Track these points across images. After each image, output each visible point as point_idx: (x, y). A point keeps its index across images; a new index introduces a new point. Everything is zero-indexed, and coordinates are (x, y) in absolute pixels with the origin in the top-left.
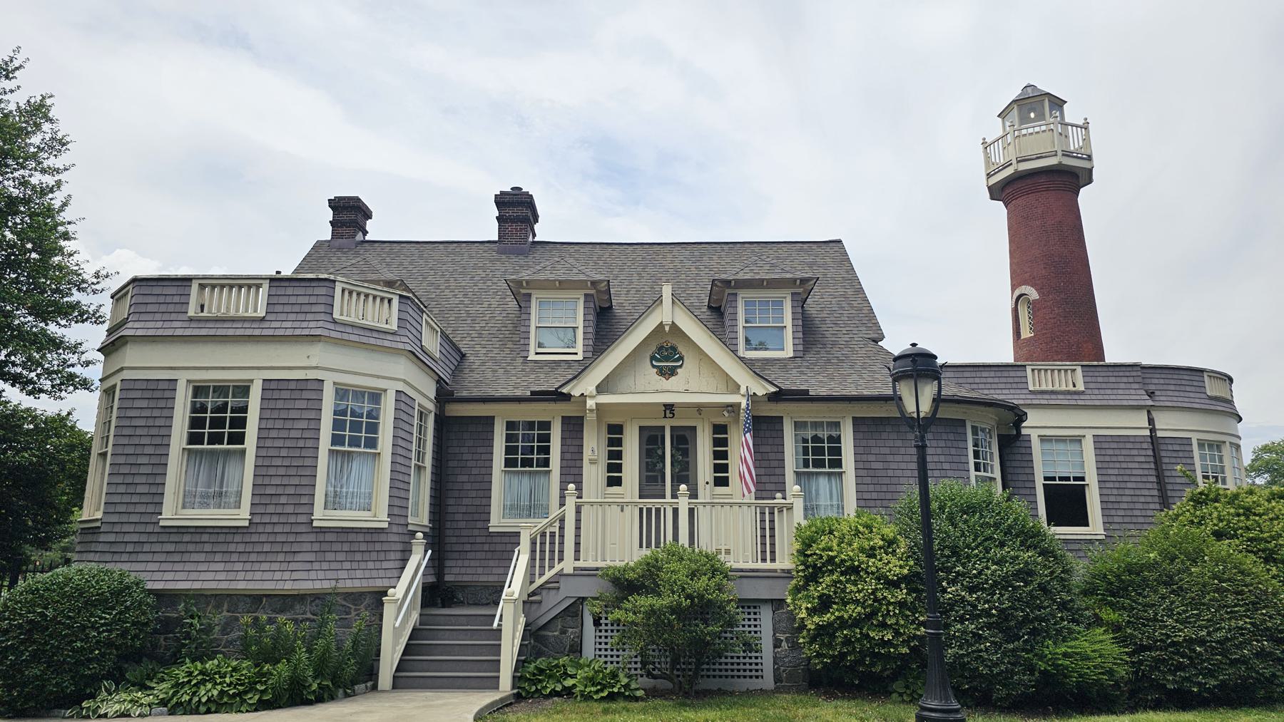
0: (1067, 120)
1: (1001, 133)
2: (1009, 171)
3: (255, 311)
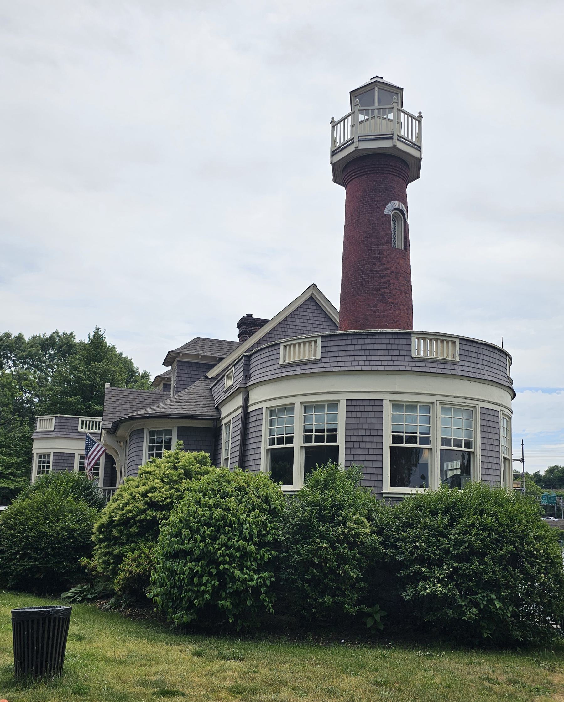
2: (352, 149)
3: (315, 355)
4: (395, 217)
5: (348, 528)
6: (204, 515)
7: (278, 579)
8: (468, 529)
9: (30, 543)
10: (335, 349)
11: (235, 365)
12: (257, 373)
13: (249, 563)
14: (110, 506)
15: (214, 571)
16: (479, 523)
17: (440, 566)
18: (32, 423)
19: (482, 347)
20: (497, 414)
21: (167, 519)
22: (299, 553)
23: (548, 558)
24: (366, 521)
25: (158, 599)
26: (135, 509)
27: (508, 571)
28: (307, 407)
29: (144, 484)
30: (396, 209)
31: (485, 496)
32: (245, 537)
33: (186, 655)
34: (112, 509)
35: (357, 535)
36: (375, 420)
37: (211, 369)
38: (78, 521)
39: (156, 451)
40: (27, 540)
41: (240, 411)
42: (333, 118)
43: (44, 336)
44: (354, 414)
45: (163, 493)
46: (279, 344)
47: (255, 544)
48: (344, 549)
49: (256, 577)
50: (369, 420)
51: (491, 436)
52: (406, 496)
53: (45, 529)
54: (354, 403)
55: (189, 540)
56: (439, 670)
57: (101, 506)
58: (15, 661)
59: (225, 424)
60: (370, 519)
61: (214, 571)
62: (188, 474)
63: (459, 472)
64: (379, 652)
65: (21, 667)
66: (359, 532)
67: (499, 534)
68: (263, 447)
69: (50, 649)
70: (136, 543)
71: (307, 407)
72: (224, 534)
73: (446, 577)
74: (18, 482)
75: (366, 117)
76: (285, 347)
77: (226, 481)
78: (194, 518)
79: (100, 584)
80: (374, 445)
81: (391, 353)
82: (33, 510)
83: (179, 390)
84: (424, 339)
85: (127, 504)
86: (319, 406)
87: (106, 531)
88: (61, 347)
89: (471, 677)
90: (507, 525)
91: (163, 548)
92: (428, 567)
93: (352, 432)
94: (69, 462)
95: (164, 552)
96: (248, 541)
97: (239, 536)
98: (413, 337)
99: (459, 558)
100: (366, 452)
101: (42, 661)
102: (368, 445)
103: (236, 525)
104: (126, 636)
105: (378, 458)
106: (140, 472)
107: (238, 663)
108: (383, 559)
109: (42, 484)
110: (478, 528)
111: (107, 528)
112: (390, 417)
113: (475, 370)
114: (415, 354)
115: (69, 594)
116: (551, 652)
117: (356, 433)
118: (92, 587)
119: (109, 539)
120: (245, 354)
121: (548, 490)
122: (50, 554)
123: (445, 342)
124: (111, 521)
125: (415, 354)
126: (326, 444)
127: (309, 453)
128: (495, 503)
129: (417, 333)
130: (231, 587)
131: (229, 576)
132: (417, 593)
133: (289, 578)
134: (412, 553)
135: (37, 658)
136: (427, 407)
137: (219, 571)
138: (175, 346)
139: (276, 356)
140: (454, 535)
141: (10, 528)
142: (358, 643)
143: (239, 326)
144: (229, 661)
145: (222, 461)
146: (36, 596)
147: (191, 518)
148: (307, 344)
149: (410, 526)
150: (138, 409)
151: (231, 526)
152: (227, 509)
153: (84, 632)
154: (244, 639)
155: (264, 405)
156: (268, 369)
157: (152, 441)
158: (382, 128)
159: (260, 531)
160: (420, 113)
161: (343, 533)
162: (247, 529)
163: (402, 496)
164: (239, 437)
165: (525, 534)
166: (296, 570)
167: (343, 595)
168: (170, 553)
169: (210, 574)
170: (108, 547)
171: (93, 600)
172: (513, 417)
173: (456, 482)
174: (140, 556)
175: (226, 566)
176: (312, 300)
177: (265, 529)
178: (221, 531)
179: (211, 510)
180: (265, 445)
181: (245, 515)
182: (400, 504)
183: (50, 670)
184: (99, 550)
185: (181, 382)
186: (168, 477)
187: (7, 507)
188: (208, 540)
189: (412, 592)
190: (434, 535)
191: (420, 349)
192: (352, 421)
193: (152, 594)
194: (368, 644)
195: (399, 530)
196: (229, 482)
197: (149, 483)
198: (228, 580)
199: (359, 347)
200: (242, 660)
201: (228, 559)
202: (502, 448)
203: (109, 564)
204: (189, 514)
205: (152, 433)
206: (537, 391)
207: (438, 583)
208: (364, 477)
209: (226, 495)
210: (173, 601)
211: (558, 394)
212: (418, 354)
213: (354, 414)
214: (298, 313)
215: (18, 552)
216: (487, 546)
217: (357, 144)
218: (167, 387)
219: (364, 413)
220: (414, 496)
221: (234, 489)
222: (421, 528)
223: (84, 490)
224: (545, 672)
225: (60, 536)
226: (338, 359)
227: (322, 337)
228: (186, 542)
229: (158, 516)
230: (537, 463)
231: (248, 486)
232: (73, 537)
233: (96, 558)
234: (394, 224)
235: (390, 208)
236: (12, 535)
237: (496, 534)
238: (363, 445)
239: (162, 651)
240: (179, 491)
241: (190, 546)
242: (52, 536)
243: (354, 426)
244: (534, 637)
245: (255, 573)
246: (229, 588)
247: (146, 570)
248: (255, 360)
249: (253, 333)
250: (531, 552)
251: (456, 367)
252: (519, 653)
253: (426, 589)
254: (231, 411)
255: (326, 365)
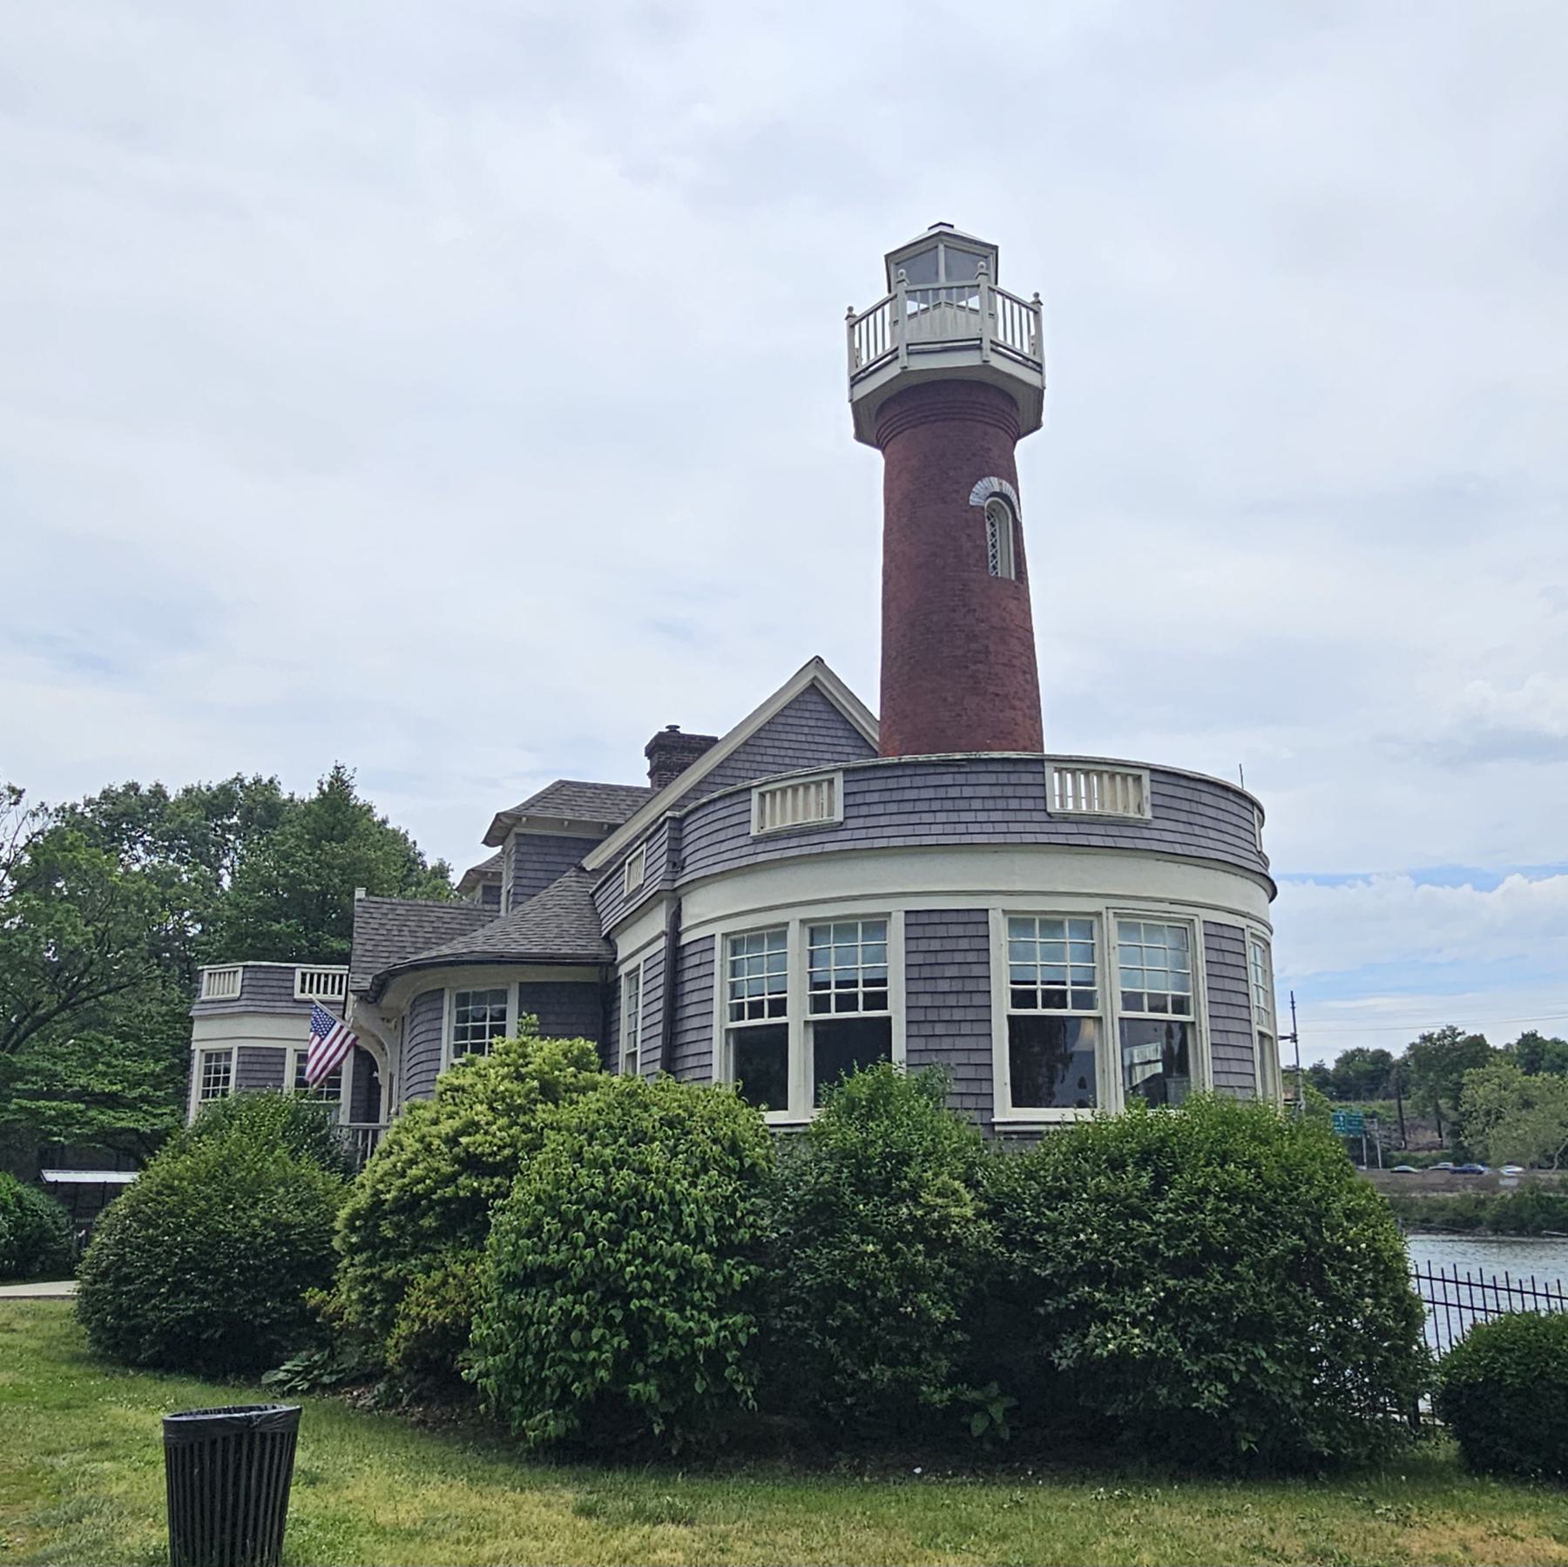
0: (1001, 285)
1: (885, 294)
2: (894, 370)
3: (831, 814)
4: (993, 512)
5: (924, 1206)
6: (592, 1186)
7: (766, 1330)
8: (1195, 1198)
9: (191, 1257)
10: (875, 797)
11: (647, 840)
12: (699, 855)
13: (697, 1296)
14: (374, 1169)
15: (618, 1315)
16: (1218, 1185)
17: (1136, 1287)
18: (191, 981)
19: (1200, 786)
20: (1239, 935)
21: (506, 1196)
22: (811, 1269)
23: (1377, 1260)
24: (962, 1190)
25: (489, 1383)
26: (432, 1175)
27: (1289, 1293)
28: (816, 930)
29: (450, 1117)
30: (994, 494)
31: (1230, 1121)
32: (687, 1235)
33: (560, 1513)
34: (378, 1175)
35: (945, 1221)
36: (971, 957)
37: (590, 851)
38: (299, 1204)
39: (473, 1039)
40: (183, 1249)
41: (662, 943)
42: (850, 309)
43: (209, 789)
44: (923, 945)
45: (494, 1135)
46: (749, 789)
47: (710, 1249)
48: (917, 1255)
49: (714, 1325)
50: (959, 957)
51: (1229, 985)
52: (1051, 1128)
53: (225, 1224)
54: (924, 919)
55: (559, 1243)
56: (1150, 1532)
57: (349, 1171)
58: (172, 1540)
59: (627, 975)
60: (971, 1183)
61: (618, 1315)
62: (549, 1091)
63: (1159, 1068)
64: (1002, 1495)
65: (186, 1554)
66: (949, 1215)
67: (1268, 1211)
68: (717, 1026)
69: (252, 1506)
70: (434, 1251)
71: (816, 930)
72: (638, 1227)
73: (1151, 1313)
74: (155, 1116)
75: (923, 306)
76: (762, 795)
77: (638, 1106)
78: (569, 1191)
79: (348, 1349)
80: (971, 1014)
81: (1001, 804)
82: (199, 1181)
83: (520, 899)
84: (1073, 772)
85: (412, 1162)
86: (845, 927)
87: (364, 1226)
88: (250, 811)
89: (1222, 1547)
90: (1282, 1187)
91: (499, 1263)
92: (1107, 1291)
93: (919, 986)
94: (273, 1068)
95: (501, 1273)
96: (694, 1243)
97: (675, 1232)
98: (1049, 768)
99: (1179, 1268)
100: (953, 1030)
101: (234, 1538)
102: (958, 1015)
103: (666, 1207)
104: (418, 1473)
105: (983, 1044)
106: (439, 1088)
107: (683, 1531)
108: (1004, 1274)
109: (216, 1119)
110: (1217, 1197)
111: (366, 1219)
112: (1006, 949)
113: (1188, 839)
114: (1054, 806)
115: (281, 1376)
116: (1399, 1478)
117: (930, 986)
118: (332, 1357)
119: (372, 1245)
120: (669, 814)
121: (1344, 1103)
122: (238, 1283)
123: (1118, 778)
124: (377, 1204)
125: (1054, 806)
126: (861, 1013)
127: (824, 1035)
128: (1253, 1137)
129: (1054, 759)
130: (657, 1351)
131: (651, 1325)
132: (1087, 1351)
133: (789, 1327)
134: (1071, 1260)
135: (223, 1531)
136: (1086, 924)
137: (628, 1315)
138: (511, 801)
139: (743, 818)
140: (1164, 1213)
141: (147, 1223)
142: (954, 1475)
143: (650, 752)
144: (660, 1528)
145: (622, 1058)
146: (205, 1381)
147: (563, 1192)
148: (813, 788)
149: (1064, 1195)
150: (428, 944)
151: (653, 1208)
152: (644, 1171)
153: (321, 1463)
154: (690, 1472)
155: (718, 929)
156: (724, 847)
157: (463, 1017)
158: (958, 327)
159: (721, 1218)
160: (1037, 295)
161: (912, 1218)
162: (691, 1215)
163: (1043, 1128)
164: (660, 1004)
165: (1324, 1205)
166: (807, 1305)
167: (917, 1362)
168: (515, 1275)
169: (609, 1322)
170: (369, 1263)
171: (333, 1388)
172: (1273, 941)
173: (1155, 1092)
174: (444, 1283)
175: (645, 1302)
176: (816, 694)
177: (733, 1215)
178: (632, 1220)
179: (607, 1173)
180: (721, 1022)
181: (686, 1183)
182: (1035, 1149)
183: (253, 1559)
184: (350, 1270)
185: (524, 882)
186: (503, 1099)
187: (135, 1175)
188: (603, 1243)
189: (1074, 1350)
190: (1119, 1216)
191: (1064, 794)
192: (918, 959)
193: (475, 1371)
194: (977, 1476)
195: (1040, 1205)
196: (646, 1108)
197: (462, 1113)
198: (651, 1334)
199: (930, 793)
200: (690, 1522)
201: (648, 1285)
202: (1254, 1012)
203: (374, 1303)
204: (558, 1185)
205: (463, 999)
206: (1304, 882)
207: (1134, 1327)
208: (956, 1088)
209: (640, 1138)
210: (523, 1385)
211: (1351, 887)
212: (1062, 805)
213: (923, 945)
214: (782, 720)
215: (162, 1280)
216: (1240, 1238)
217: (904, 360)
218: (492, 893)
219: (947, 940)
220: (1069, 1128)
221: (657, 1124)
222: (1089, 1201)
223: (309, 1132)
224: (1389, 1528)
225: (260, 1239)
226: (883, 821)
227: (846, 771)
228: (553, 1247)
229: (484, 1189)
230: (1318, 1043)
231: (691, 1115)
232: (288, 1243)
233: (344, 1289)
234: (993, 525)
235: (980, 493)
236: (153, 1241)
237: (1259, 1209)
238: (946, 1015)
239: (504, 1508)
240: (531, 1130)
241: (562, 1256)
242: (241, 1240)
243: (926, 972)
244: (1355, 1446)
245: (712, 1317)
246: (654, 1352)
247: (458, 1314)
248: (693, 827)
249: (683, 767)
250: (1340, 1249)
251: (1146, 834)
252: (1323, 1485)
253: (1106, 1342)
254: (640, 945)
255: (857, 834)
